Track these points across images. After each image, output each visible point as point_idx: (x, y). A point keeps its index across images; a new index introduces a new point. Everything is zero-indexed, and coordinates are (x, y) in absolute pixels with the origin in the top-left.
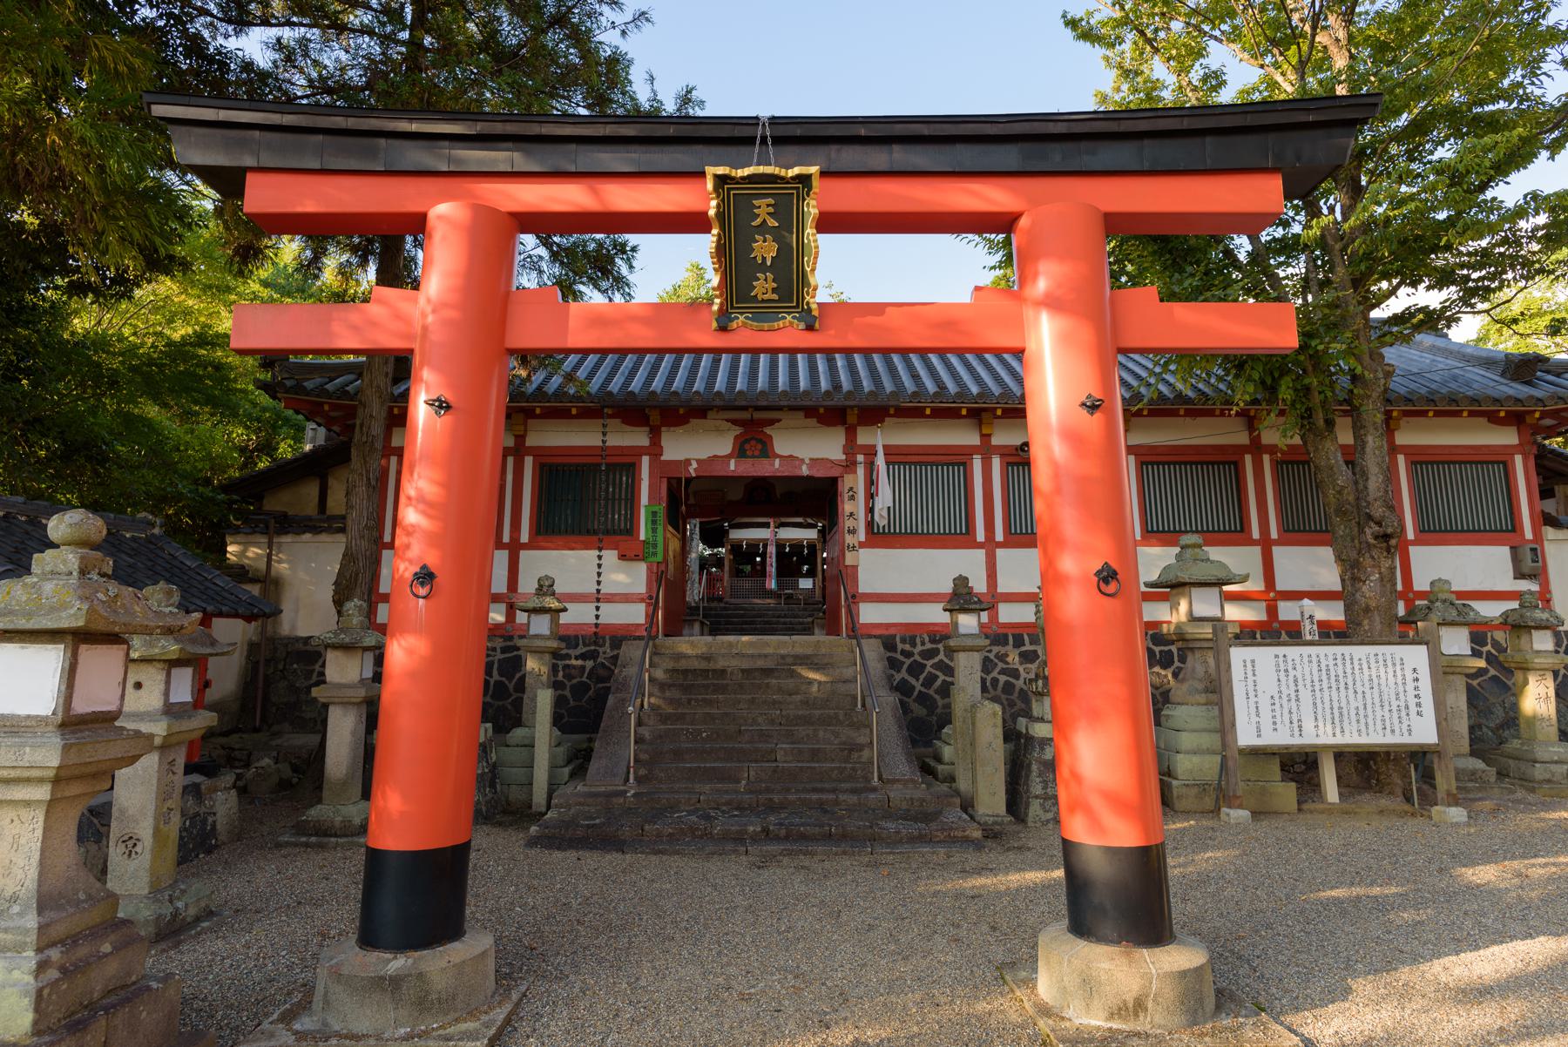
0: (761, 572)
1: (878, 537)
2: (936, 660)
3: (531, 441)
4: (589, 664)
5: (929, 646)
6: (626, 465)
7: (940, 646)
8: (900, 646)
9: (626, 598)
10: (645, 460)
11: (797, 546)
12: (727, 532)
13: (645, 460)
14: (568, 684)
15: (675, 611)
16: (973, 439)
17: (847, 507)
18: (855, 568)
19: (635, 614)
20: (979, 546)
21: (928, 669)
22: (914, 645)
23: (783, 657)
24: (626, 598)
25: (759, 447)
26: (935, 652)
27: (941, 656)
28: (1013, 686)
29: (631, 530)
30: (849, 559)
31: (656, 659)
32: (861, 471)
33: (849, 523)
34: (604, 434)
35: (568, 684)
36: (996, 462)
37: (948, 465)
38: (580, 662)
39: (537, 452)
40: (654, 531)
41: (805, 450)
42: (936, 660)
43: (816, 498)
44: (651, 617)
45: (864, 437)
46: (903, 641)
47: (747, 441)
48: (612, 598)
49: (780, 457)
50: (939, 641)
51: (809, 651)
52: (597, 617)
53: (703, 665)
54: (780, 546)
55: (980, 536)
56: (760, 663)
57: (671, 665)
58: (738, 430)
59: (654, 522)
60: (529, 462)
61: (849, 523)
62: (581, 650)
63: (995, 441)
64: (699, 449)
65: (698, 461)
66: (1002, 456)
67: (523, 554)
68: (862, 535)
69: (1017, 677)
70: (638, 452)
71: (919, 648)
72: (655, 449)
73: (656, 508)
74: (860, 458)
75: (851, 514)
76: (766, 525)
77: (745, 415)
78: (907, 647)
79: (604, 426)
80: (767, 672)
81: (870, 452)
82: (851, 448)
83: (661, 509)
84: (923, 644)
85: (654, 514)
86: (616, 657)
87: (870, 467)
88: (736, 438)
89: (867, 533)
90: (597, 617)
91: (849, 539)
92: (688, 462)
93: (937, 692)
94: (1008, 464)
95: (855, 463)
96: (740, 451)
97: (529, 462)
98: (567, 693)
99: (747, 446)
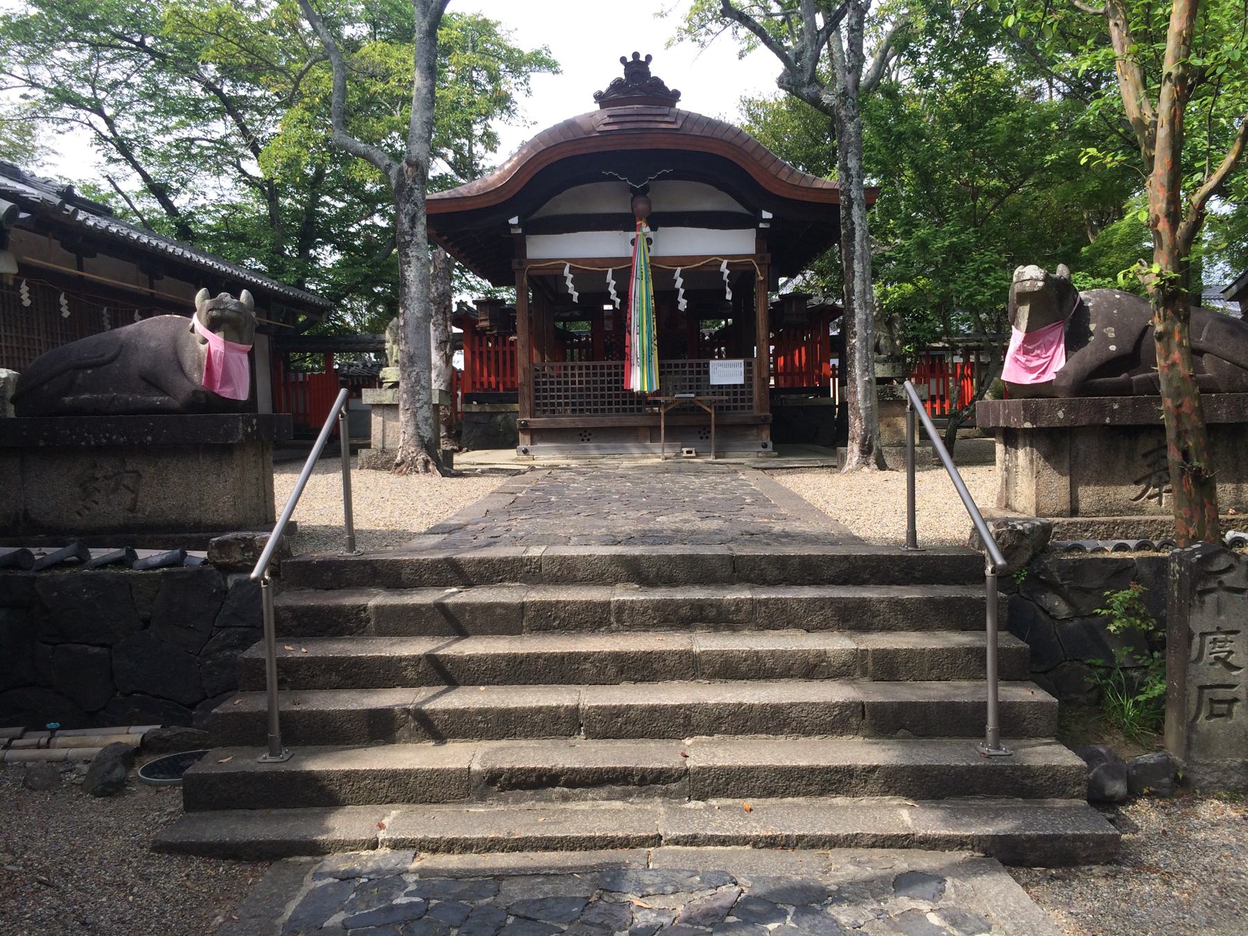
0: (611, 344)
11: (702, 274)
12: (519, 246)
54: (661, 272)
76: (623, 223)
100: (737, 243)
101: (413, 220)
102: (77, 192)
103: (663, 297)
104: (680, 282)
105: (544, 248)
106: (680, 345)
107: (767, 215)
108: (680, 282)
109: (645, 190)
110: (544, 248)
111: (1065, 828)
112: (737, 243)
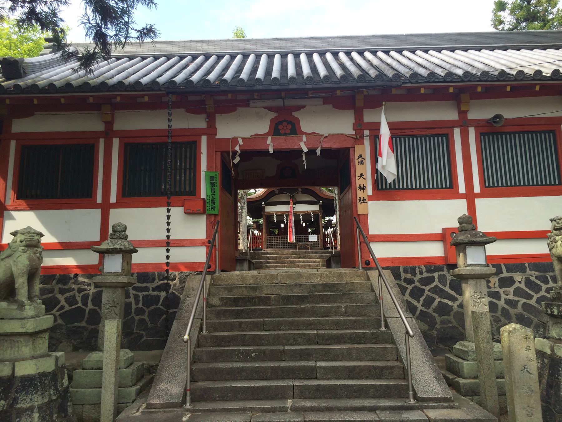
0: (284, 232)
1: (384, 190)
2: (432, 285)
3: (117, 127)
4: (163, 294)
5: (426, 275)
6: (187, 146)
7: (436, 275)
8: (403, 276)
9: (192, 243)
10: (204, 139)
11: (307, 215)
12: (263, 209)
13: (204, 139)
14: (147, 310)
15: (225, 253)
16: (452, 115)
17: (359, 169)
18: (366, 215)
19: (199, 255)
20: (461, 197)
21: (427, 293)
22: (414, 274)
23: (314, 286)
24: (192, 243)
25: (290, 127)
26: (432, 279)
27: (437, 282)
28: (496, 305)
29: (194, 191)
30: (361, 209)
31: (213, 290)
32: (367, 142)
33: (360, 182)
34: (170, 121)
35: (147, 310)
36: (472, 132)
37: (434, 136)
38: (156, 293)
39: (123, 135)
40: (213, 190)
41: (324, 127)
42: (432, 285)
43: (334, 167)
44: (209, 256)
45: (368, 117)
46: (406, 271)
47: (280, 123)
48: (180, 243)
49: (306, 134)
50: (435, 271)
51: (334, 281)
52: (168, 257)
53: (251, 294)
54: (296, 215)
55: (462, 189)
56: (296, 292)
57: (226, 295)
58: (273, 115)
59: (212, 184)
60: (116, 142)
61: (360, 182)
62: (157, 283)
63: (471, 116)
64: (243, 129)
65: (243, 139)
66: (476, 127)
67: (112, 211)
68: (370, 191)
69: (499, 298)
70: (199, 133)
71: (418, 276)
72: (211, 131)
73: (213, 174)
74: (366, 132)
75: (361, 175)
76: (287, 203)
77: (278, 103)
78: (409, 276)
79: (170, 114)
80: (302, 299)
81: (375, 129)
82: (359, 125)
83: (217, 174)
84: (421, 273)
85: (212, 178)
86: (182, 288)
87: (376, 137)
88: (272, 121)
89: (374, 189)
90: (168, 257)
91: (360, 194)
92: (235, 140)
93: (435, 311)
94: (481, 134)
95: (362, 137)
96: (275, 131)
97: (116, 142)
98: (146, 317)
99: (280, 127)
100: (315, 208)
101: (244, 203)
102: (39, 28)
103: (297, 222)
104: (301, 217)
105: (270, 209)
106: (301, 232)
107: (321, 202)
108: (301, 217)
109: (293, 196)
110: (270, 209)
111: (319, 418)
112: (315, 208)
